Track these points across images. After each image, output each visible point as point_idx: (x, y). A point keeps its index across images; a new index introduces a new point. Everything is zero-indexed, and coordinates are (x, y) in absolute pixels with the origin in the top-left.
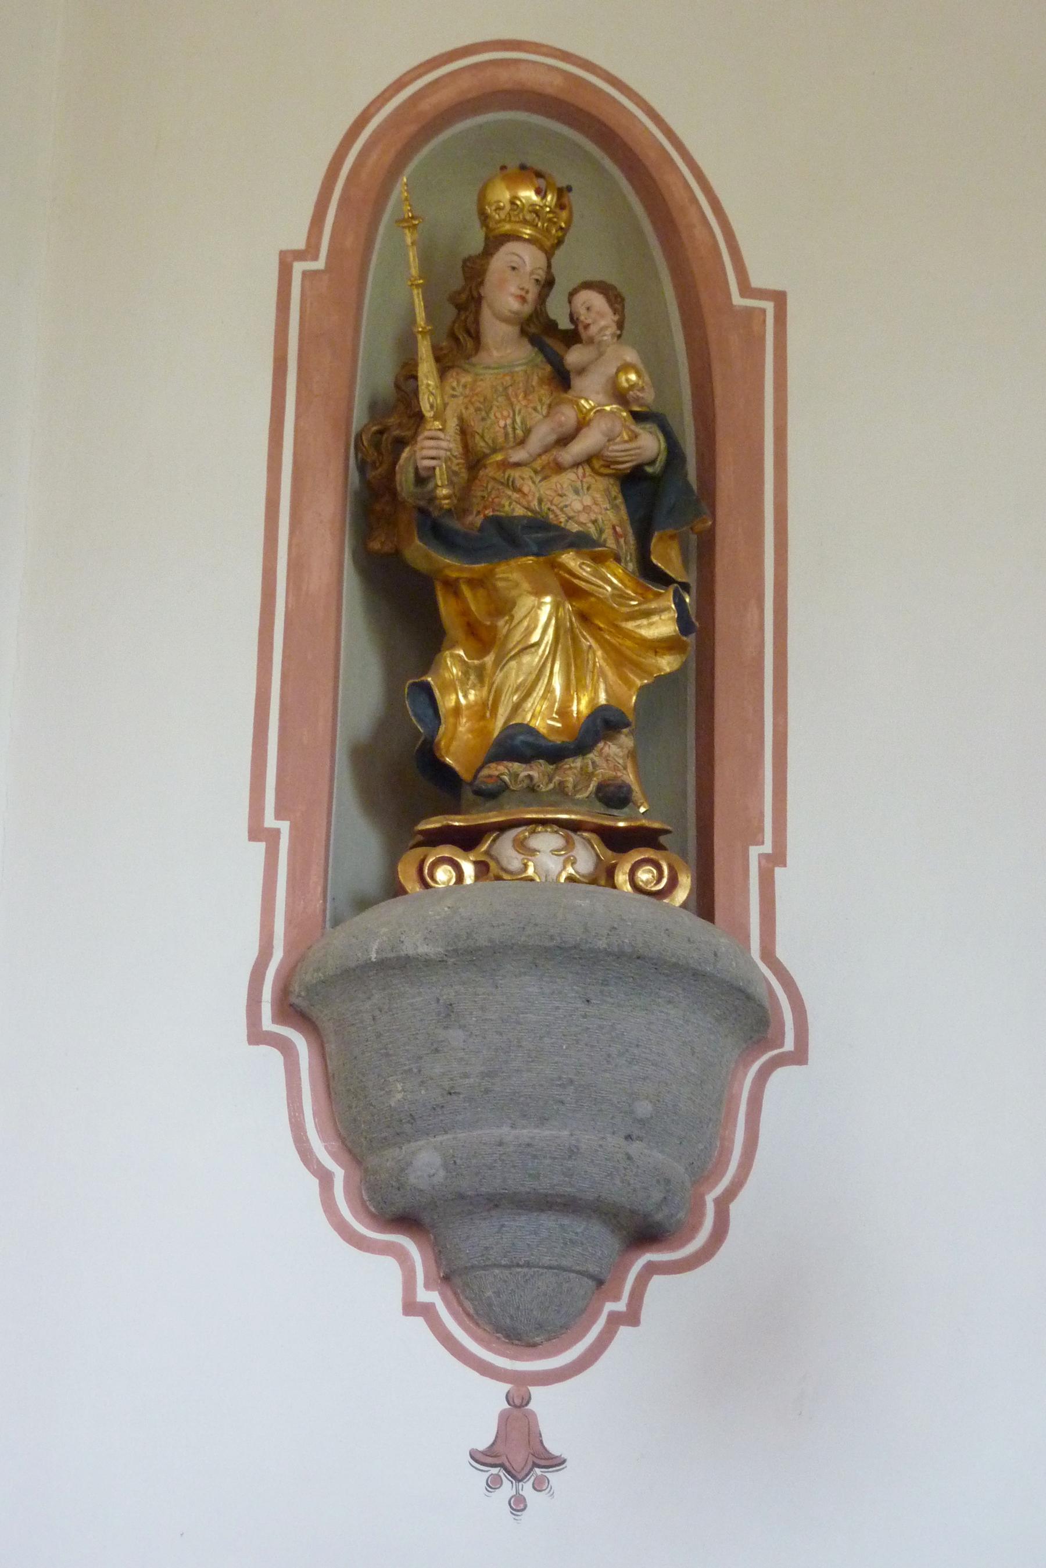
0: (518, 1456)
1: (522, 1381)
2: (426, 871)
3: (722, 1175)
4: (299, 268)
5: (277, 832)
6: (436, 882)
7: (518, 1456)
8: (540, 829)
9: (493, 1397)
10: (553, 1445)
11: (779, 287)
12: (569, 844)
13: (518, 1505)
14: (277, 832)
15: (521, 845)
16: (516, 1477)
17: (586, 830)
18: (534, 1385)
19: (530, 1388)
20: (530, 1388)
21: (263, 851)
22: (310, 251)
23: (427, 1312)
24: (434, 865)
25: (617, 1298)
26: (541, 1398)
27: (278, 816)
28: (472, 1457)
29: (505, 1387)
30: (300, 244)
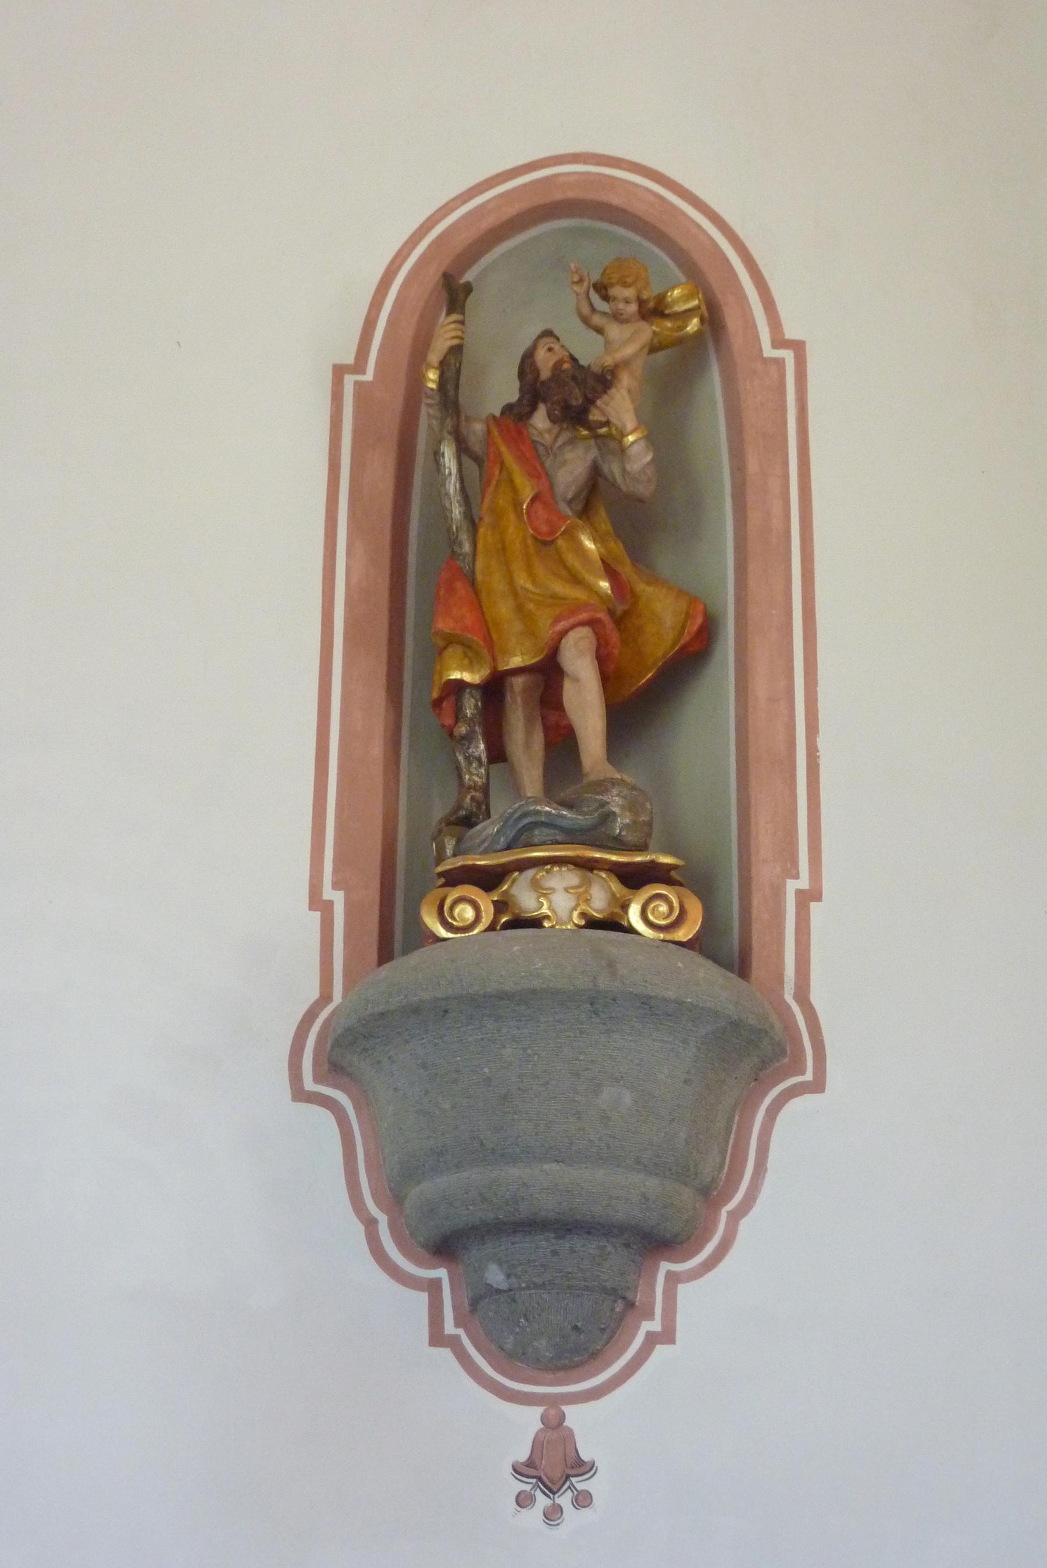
0: (554, 1471)
1: (554, 1402)
2: (446, 908)
3: (512, 1378)
4: (349, 380)
5: (331, 903)
6: (454, 919)
7: (554, 1471)
8: (556, 869)
9: (529, 1420)
10: (585, 1455)
11: (679, 1335)
12: (586, 883)
13: (553, 1515)
14: (331, 903)
15: (536, 885)
16: (551, 1491)
17: (601, 869)
18: (568, 1404)
19: (564, 1408)
20: (564, 1408)
21: (319, 917)
22: (359, 367)
23: (453, 1344)
24: (456, 902)
25: (650, 1315)
26: (575, 1416)
27: (336, 886)
28: (515, 1470)
29: (538, 1411)
30: (350, 359)
